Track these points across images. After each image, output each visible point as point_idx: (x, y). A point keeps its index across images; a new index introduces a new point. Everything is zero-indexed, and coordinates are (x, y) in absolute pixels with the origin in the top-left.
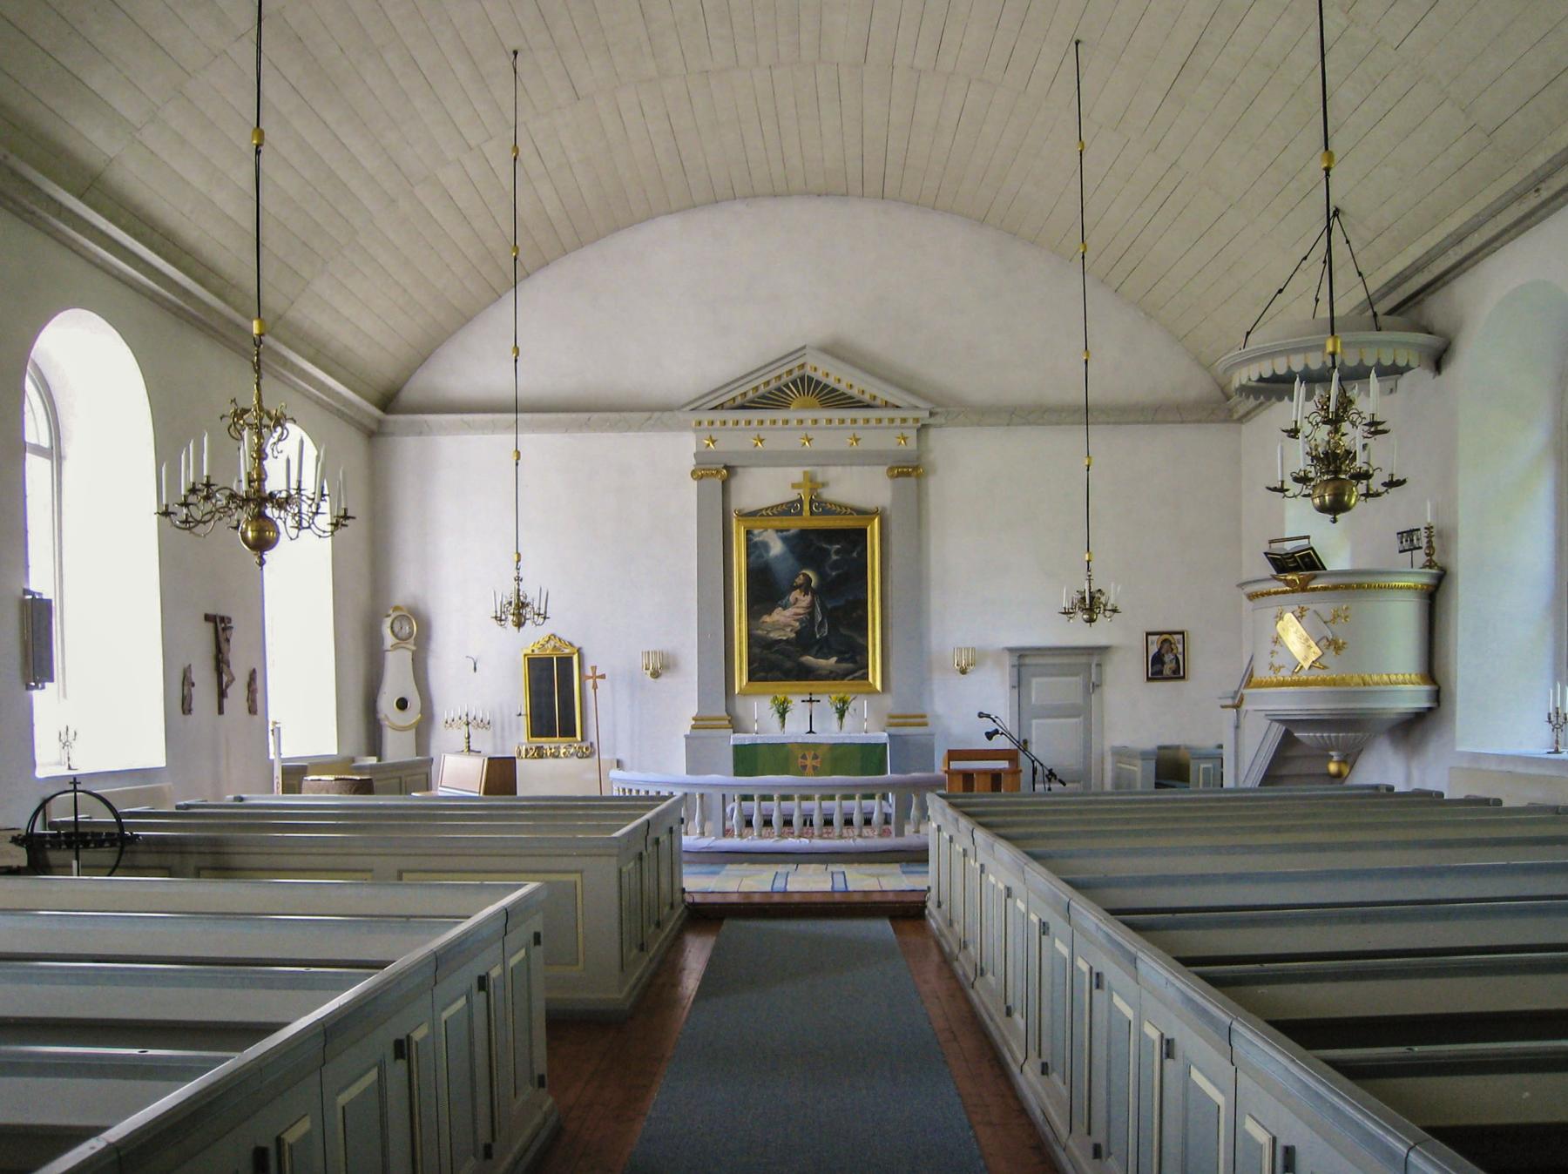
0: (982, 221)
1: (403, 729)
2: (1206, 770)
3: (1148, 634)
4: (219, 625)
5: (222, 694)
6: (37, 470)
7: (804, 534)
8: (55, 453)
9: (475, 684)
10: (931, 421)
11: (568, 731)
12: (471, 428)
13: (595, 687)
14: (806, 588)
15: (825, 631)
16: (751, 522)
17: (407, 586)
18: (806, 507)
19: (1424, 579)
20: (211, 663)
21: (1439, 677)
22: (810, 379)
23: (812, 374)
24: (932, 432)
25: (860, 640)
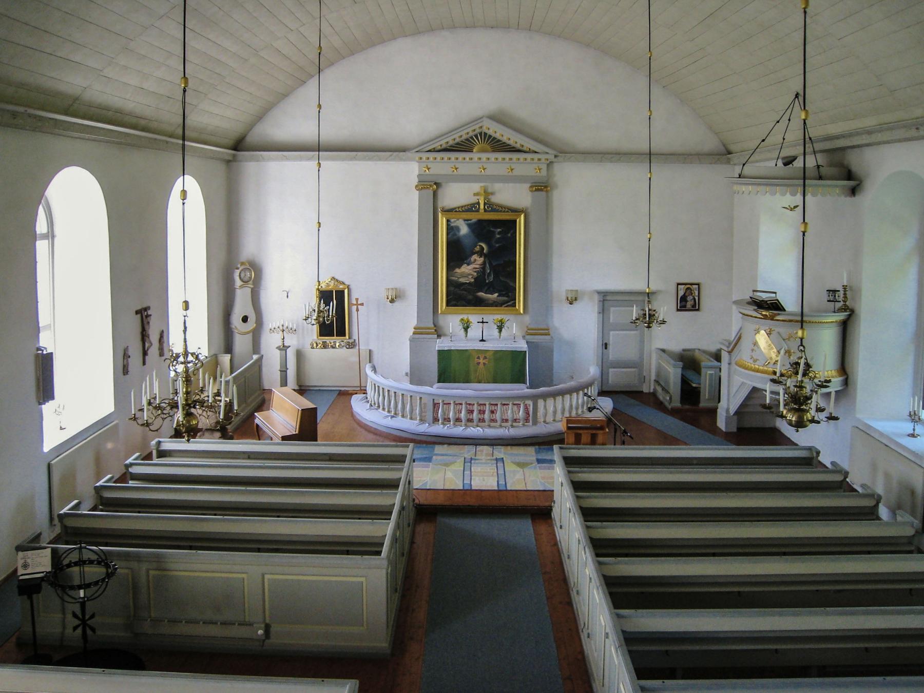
0: (588, 45)
1: (248, 333)
2: (711, 375)
3: (678, 284)
4: (143, 314)
5: (145, 353)
6: (42, 247)
7: (480, 222)
8: (50, 235)
9: (288, 301)
10: (556, 160)
11: (341, 333)
12: (287, 159)
13: (357, 310)
14: (481, 253)
15: (491, 278)
16: (450, 215)
17: (249, 249)
18: (482, 207)
19: (841, 316)
20: (139, 337)
21: (848, 370)
22: (485, 134)
23: (487, 131)
24: (555, 164)
25: (512, 284)
